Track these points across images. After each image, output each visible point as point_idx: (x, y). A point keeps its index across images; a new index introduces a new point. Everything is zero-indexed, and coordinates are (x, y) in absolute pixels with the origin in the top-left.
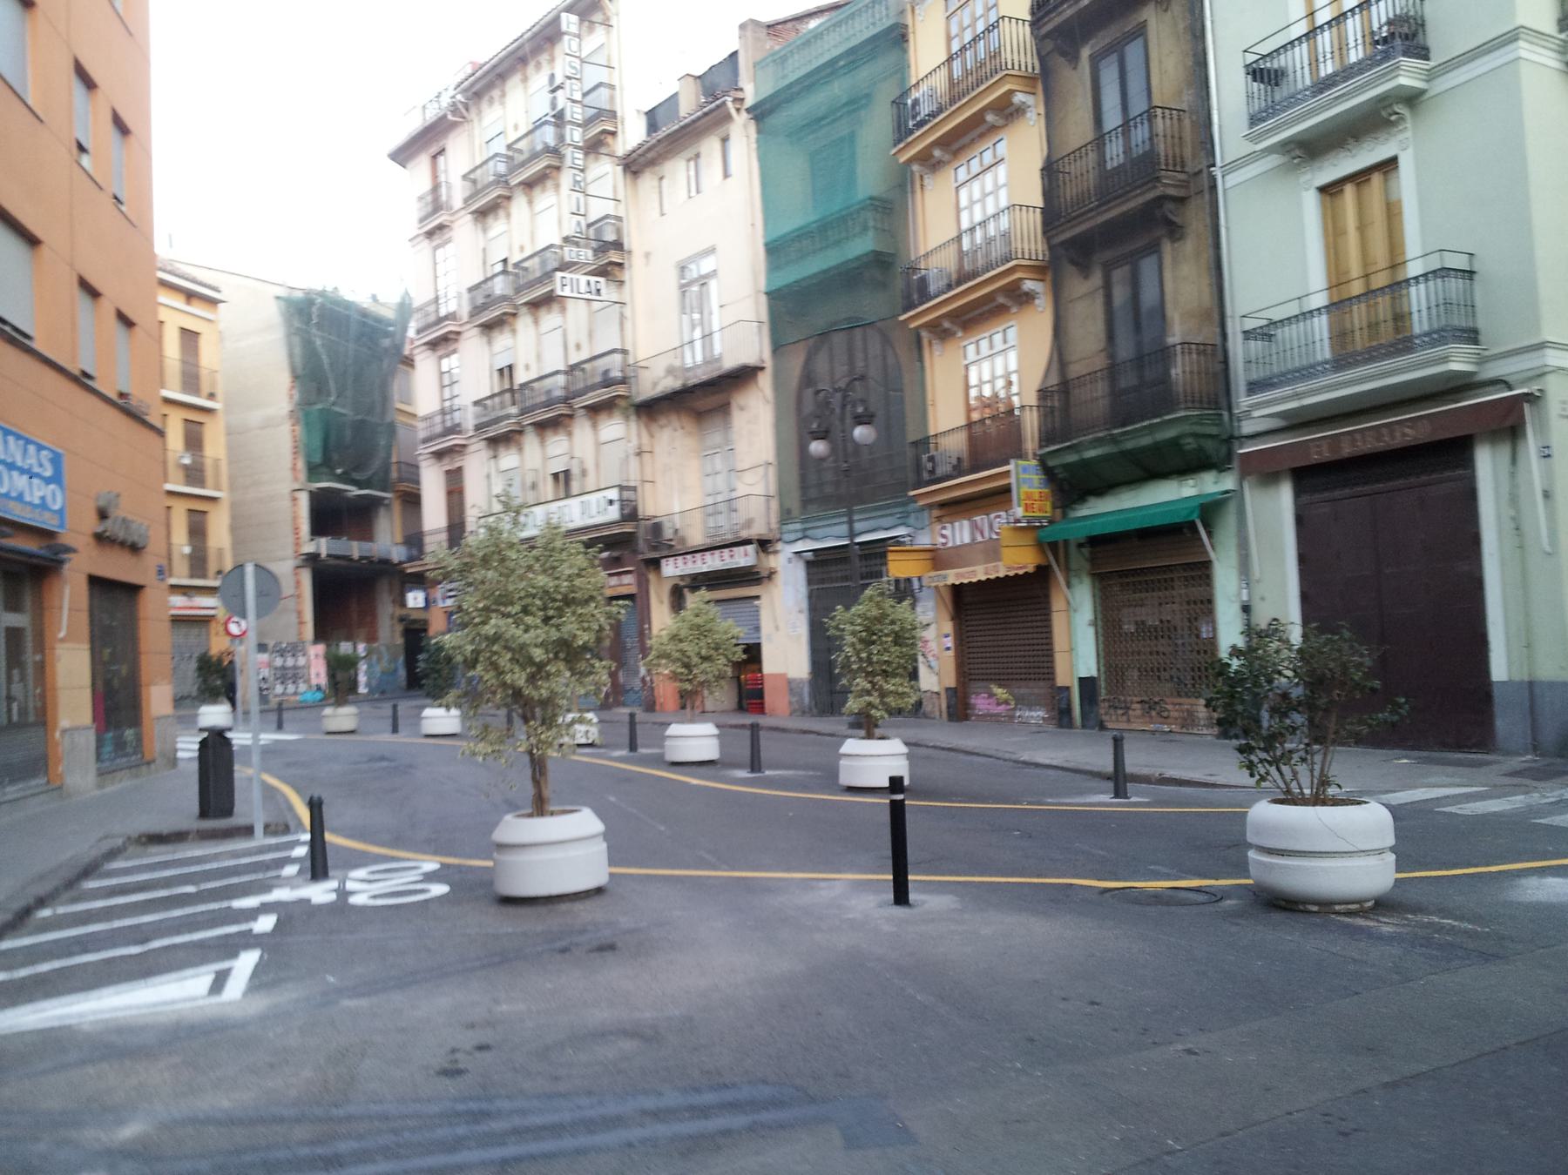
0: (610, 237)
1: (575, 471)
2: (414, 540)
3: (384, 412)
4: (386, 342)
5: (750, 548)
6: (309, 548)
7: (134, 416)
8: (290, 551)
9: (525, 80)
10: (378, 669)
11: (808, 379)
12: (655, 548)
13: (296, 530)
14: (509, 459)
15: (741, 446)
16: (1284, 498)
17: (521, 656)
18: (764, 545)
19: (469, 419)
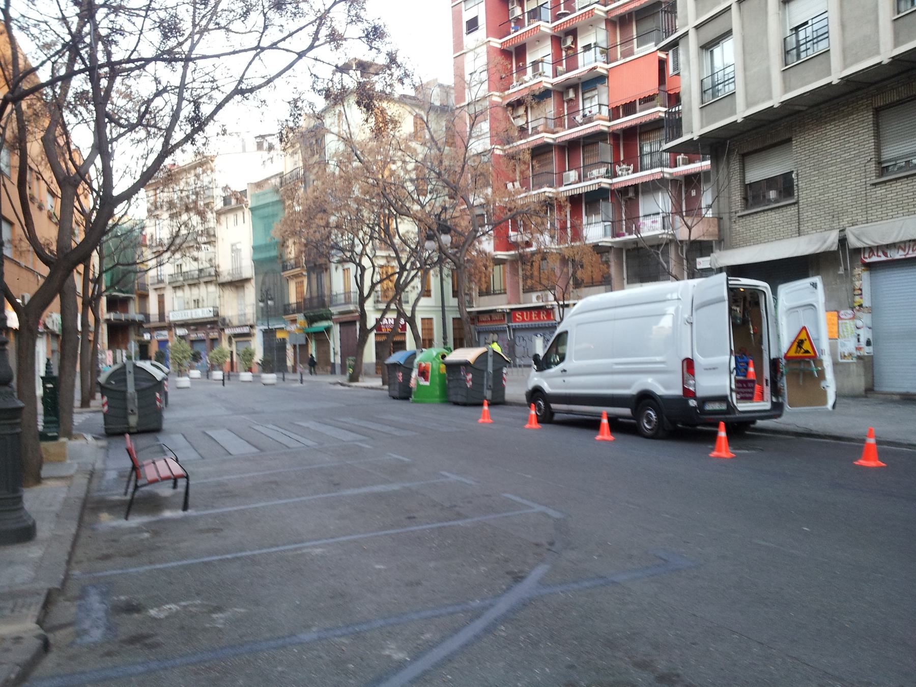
11: (263, 283)
14: (179, 293)
16: (338, 326)
18: (251, 327)
19: (167, 280)
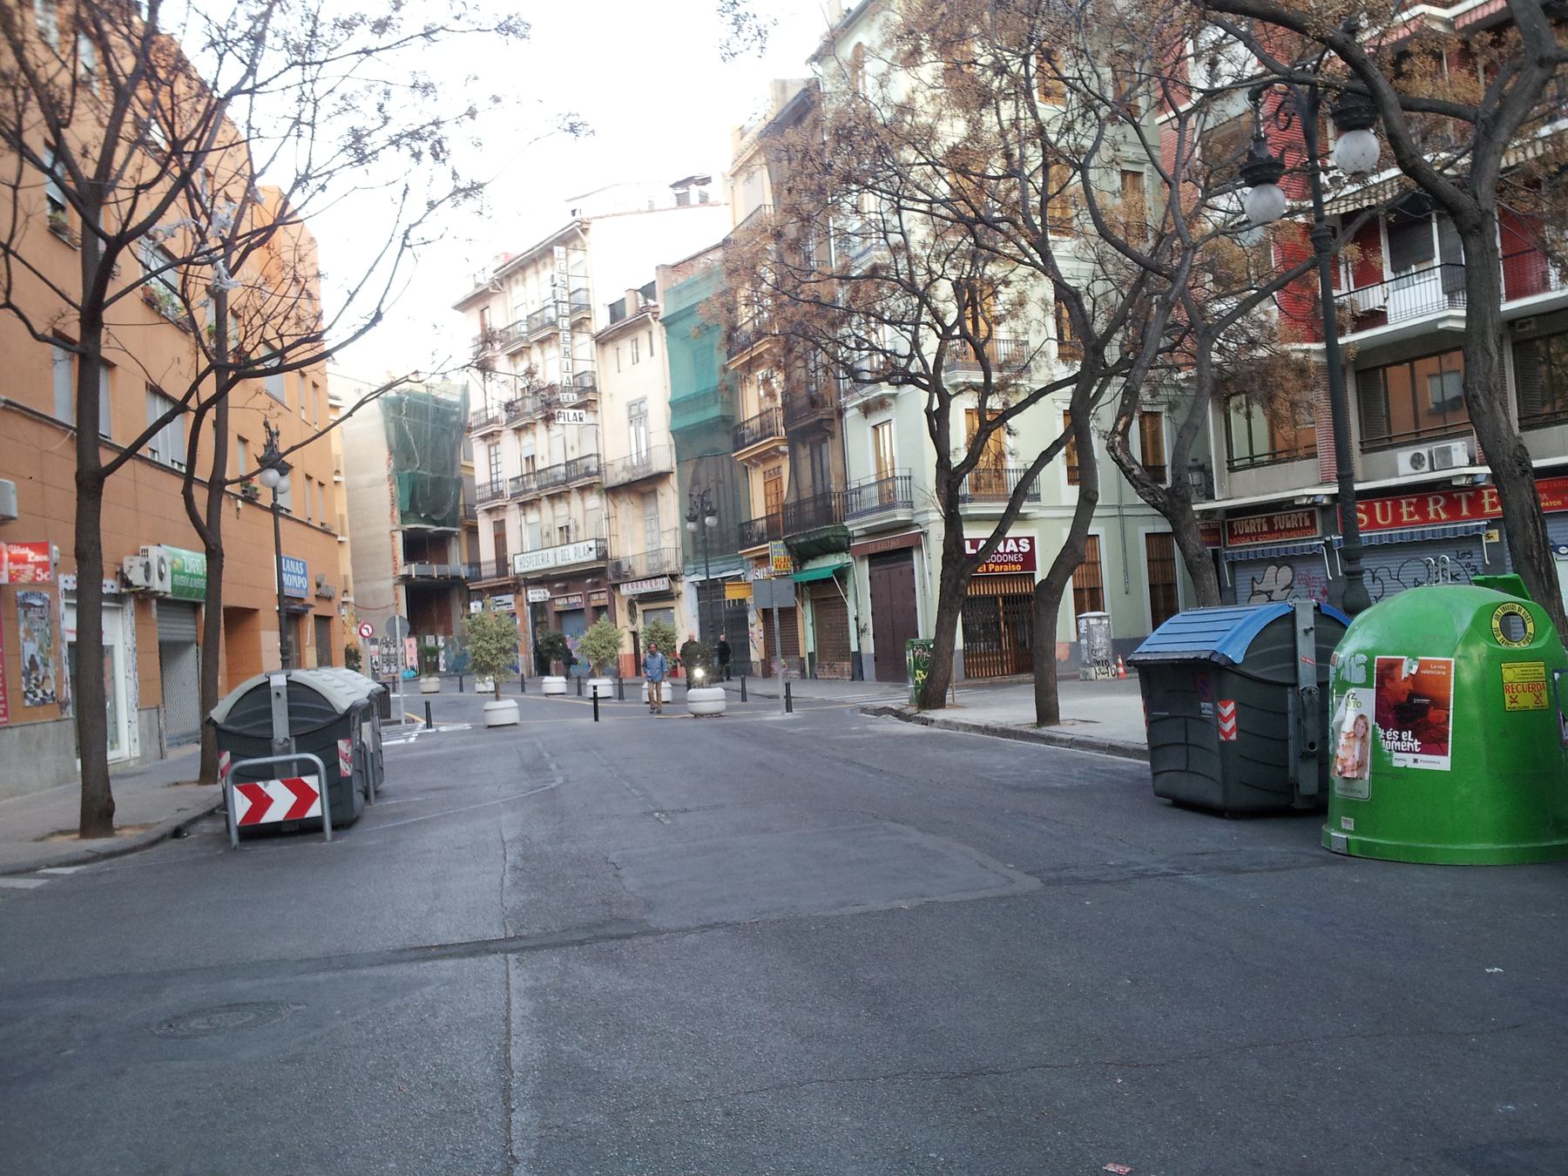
0: (588, 384)
1: (572, 527)
2: (475, 564)
3: (453, 469)
4: (454, 418)
5: (665, 580)
6: (404, 571)
7: (327, 532)
8: (390, 573)
9: (537, 272)
10: (453, 655)
11: (695, 481)
12: (618, 577)
13: (395, 558)
14: (533, 516)
15: (663, 517)
17: (488, 652)
18: (674, 577)
